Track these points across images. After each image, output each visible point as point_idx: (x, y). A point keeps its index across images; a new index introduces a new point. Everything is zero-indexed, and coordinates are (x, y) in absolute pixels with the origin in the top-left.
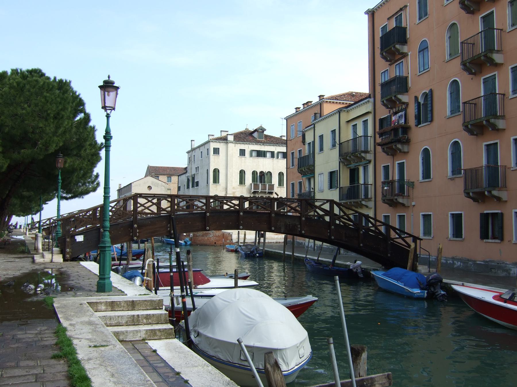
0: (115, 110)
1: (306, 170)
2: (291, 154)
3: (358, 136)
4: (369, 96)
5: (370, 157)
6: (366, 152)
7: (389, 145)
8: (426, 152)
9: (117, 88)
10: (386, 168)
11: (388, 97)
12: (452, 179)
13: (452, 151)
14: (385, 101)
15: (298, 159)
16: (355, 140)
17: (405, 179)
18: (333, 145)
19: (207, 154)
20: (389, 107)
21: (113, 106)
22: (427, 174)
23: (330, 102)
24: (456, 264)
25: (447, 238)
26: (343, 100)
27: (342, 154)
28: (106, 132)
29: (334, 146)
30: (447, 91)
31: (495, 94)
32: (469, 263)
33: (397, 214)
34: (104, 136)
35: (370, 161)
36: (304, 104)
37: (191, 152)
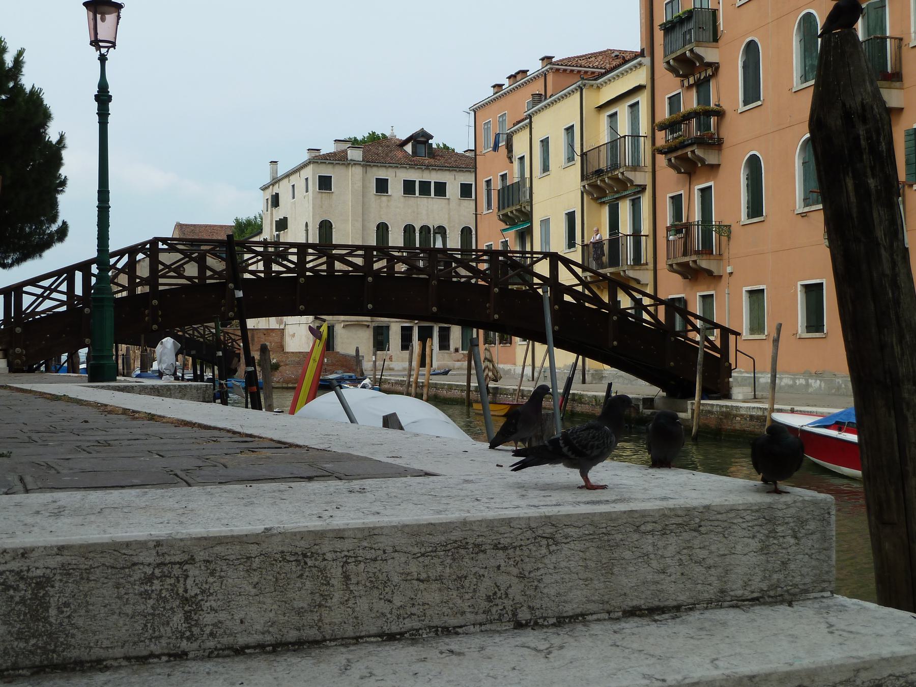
0: (115, 49)
1: (514, 213)
2: (484, 184)
3: (619, 137)
4: (642, 54)
5: (641, 178)
6: (636, 167)
7: (680, 153)
8: (754, 164)
9: (119, 7)
10: (677, 201)
11: (679, 53)
12: (803, 215)
13: (804, 158)
14: (672, 62)
15: (499, 191)
16: (613, 145)
17: (713, 220)
18: (569, 159)
19: (305, 190)
20: (681, 73)
21: (113, 40)
22: (755, 209)
23: (565, 70)
24: (811, 386)
25: (794, 334)
26: (593, 67)
27: (587, 176)
28: (99, 87)
29: (571, 159)
30: (794, 35)
31: (884, 39)
32: (837, 380)
33: (698, 294)
34: (95, 96)
35: (643, 188)
36: (509, 78)
37: (271, 187)
